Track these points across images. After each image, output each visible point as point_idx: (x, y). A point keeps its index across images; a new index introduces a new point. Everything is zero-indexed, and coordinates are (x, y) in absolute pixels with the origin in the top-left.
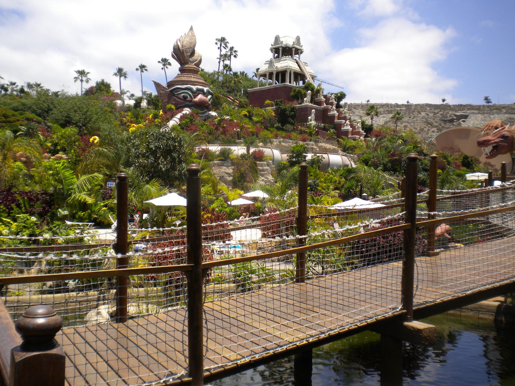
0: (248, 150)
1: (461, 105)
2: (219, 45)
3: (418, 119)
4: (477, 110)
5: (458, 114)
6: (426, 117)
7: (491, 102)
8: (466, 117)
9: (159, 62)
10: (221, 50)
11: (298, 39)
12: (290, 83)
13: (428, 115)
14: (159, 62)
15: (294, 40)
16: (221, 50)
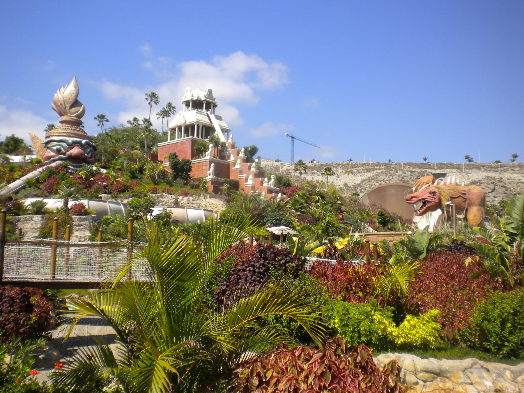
0: (66, 203)
1: (442, 164)
2: (149, 101)
3: (395, 177)
4: (456, 168)
5: (436, 172)
6: (403, 175)
7: (473, 161)
8: (444, 175)
9: (95, 118)
10: (151, 106)
11: (210, 92)
12: (202, 137)
13: (405, 173)
14: (95, 118)
15: (206, 93)
16: (151, 106)
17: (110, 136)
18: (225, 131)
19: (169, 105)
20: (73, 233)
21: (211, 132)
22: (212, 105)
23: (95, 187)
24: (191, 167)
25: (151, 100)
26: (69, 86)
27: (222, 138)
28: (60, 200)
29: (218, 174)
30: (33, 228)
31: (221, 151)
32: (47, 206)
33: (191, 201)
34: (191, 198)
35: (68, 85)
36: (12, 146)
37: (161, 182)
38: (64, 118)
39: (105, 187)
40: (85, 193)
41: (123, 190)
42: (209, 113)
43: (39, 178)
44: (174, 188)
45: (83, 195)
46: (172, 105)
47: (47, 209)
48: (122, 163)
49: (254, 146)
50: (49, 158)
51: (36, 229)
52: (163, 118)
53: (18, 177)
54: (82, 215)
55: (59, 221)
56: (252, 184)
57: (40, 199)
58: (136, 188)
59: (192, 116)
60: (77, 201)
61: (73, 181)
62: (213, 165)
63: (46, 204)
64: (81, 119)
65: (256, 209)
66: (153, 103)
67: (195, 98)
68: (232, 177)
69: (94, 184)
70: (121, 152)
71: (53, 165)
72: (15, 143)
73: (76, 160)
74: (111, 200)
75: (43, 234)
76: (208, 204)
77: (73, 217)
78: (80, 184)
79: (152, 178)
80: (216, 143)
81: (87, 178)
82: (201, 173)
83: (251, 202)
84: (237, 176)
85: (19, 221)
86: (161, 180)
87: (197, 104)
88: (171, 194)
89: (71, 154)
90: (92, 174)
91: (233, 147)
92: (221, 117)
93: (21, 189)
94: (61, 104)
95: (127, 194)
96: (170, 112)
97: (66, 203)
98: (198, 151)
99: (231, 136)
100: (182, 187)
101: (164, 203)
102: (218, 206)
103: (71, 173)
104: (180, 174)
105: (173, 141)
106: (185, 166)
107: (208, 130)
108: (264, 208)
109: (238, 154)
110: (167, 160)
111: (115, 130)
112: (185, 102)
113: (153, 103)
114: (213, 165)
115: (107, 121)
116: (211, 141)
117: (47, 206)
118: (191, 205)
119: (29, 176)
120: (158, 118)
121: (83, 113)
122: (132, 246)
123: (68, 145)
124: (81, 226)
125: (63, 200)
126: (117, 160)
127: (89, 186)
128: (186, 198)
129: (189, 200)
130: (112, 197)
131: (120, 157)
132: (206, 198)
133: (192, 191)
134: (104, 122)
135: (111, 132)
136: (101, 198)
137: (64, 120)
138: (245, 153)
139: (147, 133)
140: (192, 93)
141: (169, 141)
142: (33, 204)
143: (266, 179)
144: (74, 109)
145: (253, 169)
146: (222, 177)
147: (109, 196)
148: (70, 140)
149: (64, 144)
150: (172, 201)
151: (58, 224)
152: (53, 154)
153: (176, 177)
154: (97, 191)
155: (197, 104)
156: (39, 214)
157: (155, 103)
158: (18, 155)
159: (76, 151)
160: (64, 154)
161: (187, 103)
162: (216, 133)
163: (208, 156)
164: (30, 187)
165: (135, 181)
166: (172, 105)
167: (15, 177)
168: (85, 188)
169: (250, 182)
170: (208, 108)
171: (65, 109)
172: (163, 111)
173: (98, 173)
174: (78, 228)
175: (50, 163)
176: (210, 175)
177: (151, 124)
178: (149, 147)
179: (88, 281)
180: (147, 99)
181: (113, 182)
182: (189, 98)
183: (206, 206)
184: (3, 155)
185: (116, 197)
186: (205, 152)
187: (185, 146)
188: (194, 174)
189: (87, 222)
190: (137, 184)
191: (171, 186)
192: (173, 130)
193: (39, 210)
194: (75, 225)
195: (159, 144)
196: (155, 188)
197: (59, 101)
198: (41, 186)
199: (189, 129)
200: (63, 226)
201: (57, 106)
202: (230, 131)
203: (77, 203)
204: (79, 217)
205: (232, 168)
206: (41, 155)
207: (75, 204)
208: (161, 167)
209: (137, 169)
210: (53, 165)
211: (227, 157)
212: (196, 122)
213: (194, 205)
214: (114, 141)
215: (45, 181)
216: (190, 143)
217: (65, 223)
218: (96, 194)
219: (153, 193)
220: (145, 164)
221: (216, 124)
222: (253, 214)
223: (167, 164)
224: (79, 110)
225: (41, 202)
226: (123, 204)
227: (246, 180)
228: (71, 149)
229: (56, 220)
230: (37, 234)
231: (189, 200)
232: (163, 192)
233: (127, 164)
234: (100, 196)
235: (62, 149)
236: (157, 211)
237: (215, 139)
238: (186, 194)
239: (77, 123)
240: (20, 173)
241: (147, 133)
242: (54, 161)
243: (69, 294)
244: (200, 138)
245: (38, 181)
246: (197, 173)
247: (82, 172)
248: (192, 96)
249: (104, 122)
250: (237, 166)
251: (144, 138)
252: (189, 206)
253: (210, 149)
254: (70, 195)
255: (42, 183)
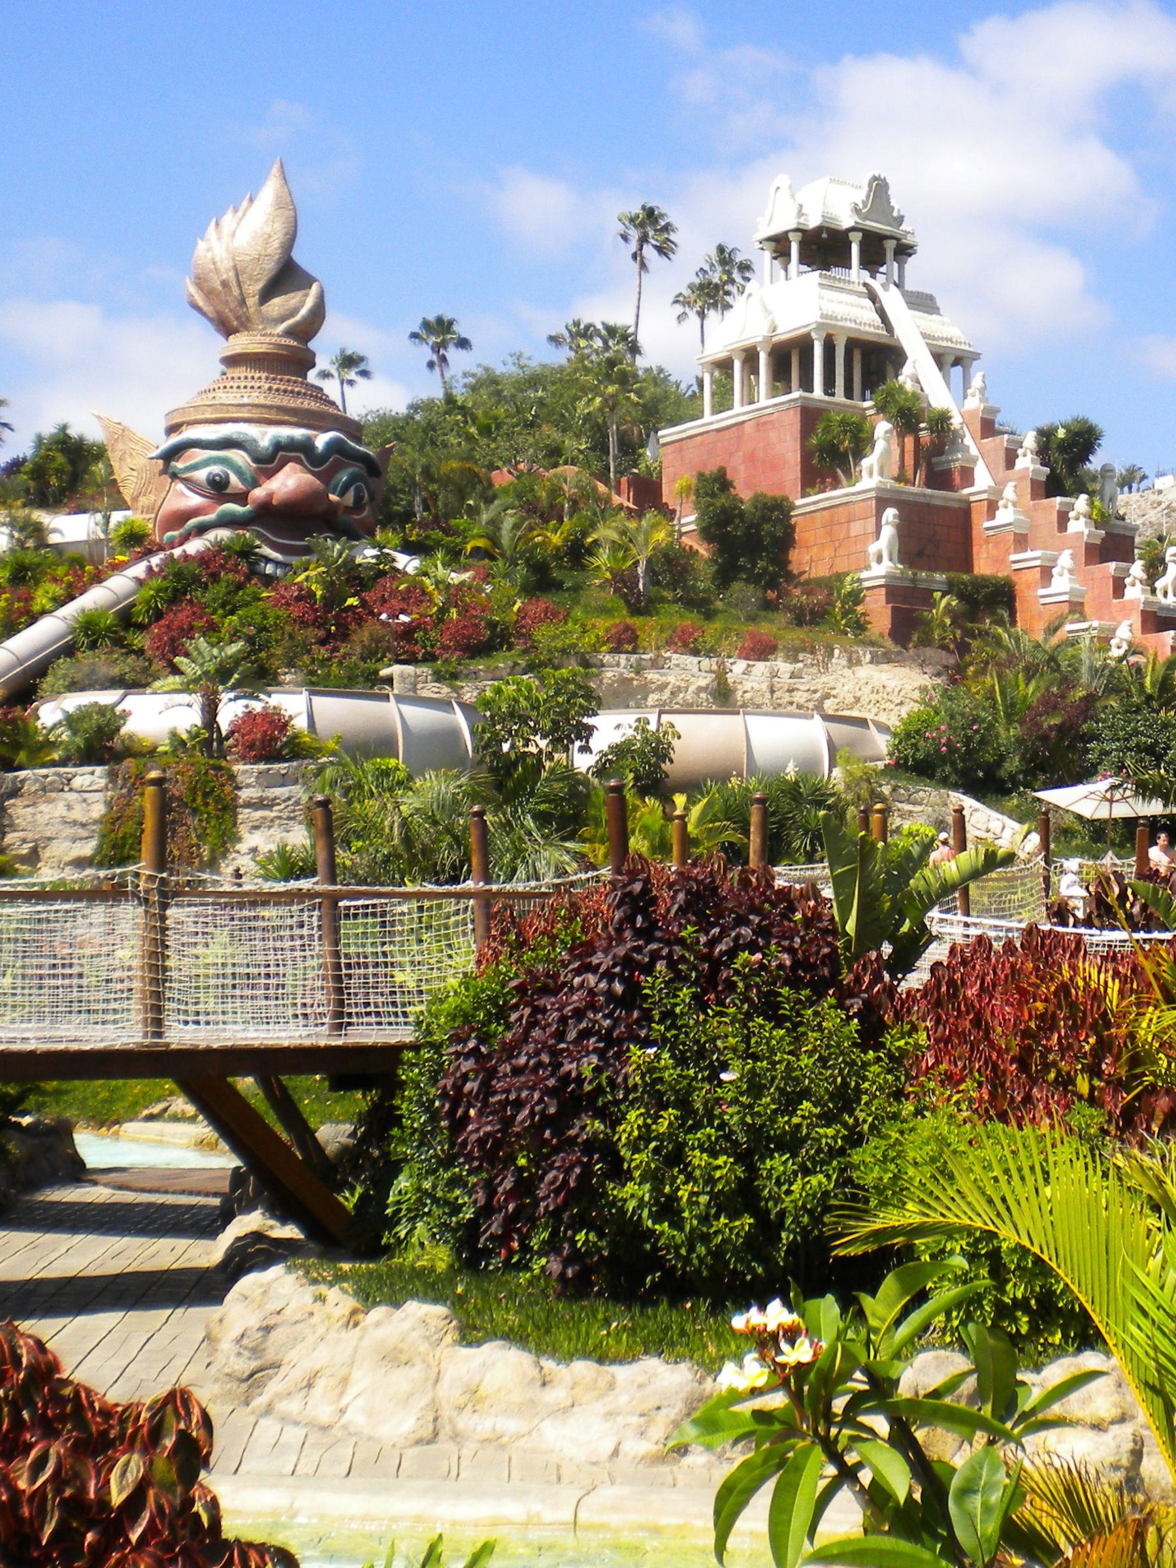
0: (211, 710)
2: (633, 246)
9: (414, 336)
10: (643, 266)
11: (879, 188)
12: (849, 394)
14: (414, 336)
15: (860, 195)
17: (463, 409)
18: (950, 360)
19: (725, 257)
20: (239, 840)
21: (890, 370)
22: (890, 245)
23: (363, 635)
24: (792, 528)
25: (644, 239)
26: (256, 203)
27: (937, 392)
28: (185, 698)
29: (920, 554)
30: (75, 823)
31: (932, 447)
32: (130, 727)
33: (785, 680)
34: (783, 667)
35: (251, 200)
36: (58, 471)
37: (663, 600)
38: (242, 343)
39: (407, 633)
40: (325, 662)
41: (483, 642)
42: (876, 284)
43: (133, 605)
44: (718, 625)
45: (312, 673)
46: (739, 258)
47: (131, 737)
48: (495, 523)
49: (1085, 421)
50: (180, 518)
51: (83, 825)
52: (702, 315)
53: (48, 606)
54: (277, 758)
55: (177, 789)
56: (1071, 592)
57: (107, 698)
58: (543, 634)
59: (792, 302)
60: (257, 698)
61: (271, 614)
62: (890, 513)
63: (125, 715)
64: (312, 345)
65: (1050, 704)
66: (649, 252)
67: (813, 222)
68: (983, 566)
69: (360, 621)
70: (502, 478)
71: (194, 547)
72: (72, 462)
73: (292, 520)
74: (431, 689)
75: (114, 847)
76: (867, 690)
77: (238, 768)
78: (304, 624)
79: (623, 581)
80: (907, 415)
81: (334, 597)
82: (842, 551)
83: (1031, 672)
84: (1002, 561)
85: (15, 793)
86: (665, 595)
87: (823, 248)
88: (695, 652)
89: (270, 495)
90: (358, 578)
91: (988, 428)
92: (931, 298)
93: (56, 655)
94: (225, 284)
95: (502, 661)
96: (734, 289)
97: (211, 710)
98: (830, 454)
99: (977, 382)
100: (752, 618)
101: (666, 694)
102: (890, 692)
103: (268, 580)
104: (742, 561)
105: (726, 418)
106: (767, 527)
107: (875, 360)
108: (1090, 699)
109: (1010, 459)
110: (689, 505)
111: (489, 383)
112: (769, 239)
113: (649, 252)
114: (890, 513)
115: (463, 343)
116: (881, 409)
117: (130, 727)
118: (787, 698)
119: (94, 598)
120: (681, 318)
121: (318, 314)
122: (163, 895)
123: (256, 460)
124: (269, 807)
125: (197, 699)
126: (473, 512)
127: (342, 637)
128: (761, 667)
129: (774, 675)
130: (439, 677)
131: (489, 501)
132: (859, 663)
133: (797, 635)
134: (452, 353)
135: (474, 388)
136: (389, 680)
137: (239, 350)
138: (1043, 452)
139: (611, 389)
140: (800, 197)
141: (708, 417)
142: (71, 721)
143: (1137, 569)
144: (277, 304)
145: (1078, 526)
146: (932, 568)
147: (425, 670)
148: (265, 436)
149: (239, 457)
150: (703, 683)
151: (164, 806)
152: (195, 500)
153: (725, 575)
154: (374, 653)
155: (823, 248)
156: (100, 762)
157: (661, 250)
158: (85, 512)
159: (289, 481)
160: (241, 498)
161: (779, 245)
162: (907, 370)
163: (874, 472)
164: (93, 646)
165: (548, 600)
166: (739, 258)
167: (36, 608)
168: (322, 642)
169: (1062, 584)
170: (873, 259)
171: (243, 302)
172: (702, 287)
173: (383, 572)
174: (259, 814)
175: (185, 539)
176: (879, 559)
177: (635, 349)
178: (630, 448)
179: (61, 1047)
180: (625, 238)
181: (443, 610)
182: (784, 222)
183: (858, 700)
184: (22, 513)
185: (455, 676)
186: (859, 454)
187: (773, 435)
188: (810, 559)
189: (298, 791)
190: (550, 615)
191: (709, 615)
192: (724, 366)
193: (100, 744)
194: (248, 805)
195: (667, 434)
196: (627, 628)
197: (217, 270)
198: (139, 640)
199: (788, 359)
200: (195, 811)
201: (209, 294)
202: (976, 356)
203: (257, 706)
204: (262, 767)
205: (982, 525)
206: (149, 509)
207: (249, 715)
208: (660, 536)
209: (558, 549)
210: (194, 547)
211: (957, 477)
212: (820, 326)
213: (800, 697)
214: (473, 430)
215: (158, 615)
216: (792, 423)
217: (206, 795)
218: (370, 665)
219: (617, 650)
220: (593, 525)
221: (910, 331)
222: (1039, 726)
223: (689, 520)
224: (303, 303)
225: (102, 710)
226: (462, 705)
227: (1046, 573)
228: (270, 474)
229: (158, 782)
230: (87, 849)
231: (774, 675)
232: (669, 643)
233: (516, 527)
234: (384, 672)
235: (233, 478)
236: (610, 729)
237: (901, 399)
238: (761, 651)
239: (292, 361)
240: (57, 590)
241: (611, 389)
242: (202, 530)
243: (159, 1100)
244: (840, 397)
245: (126, 618)
246: (828, 553)
247: (312, 573)
248: (800, 213)
249: (452, 353)
250: (1005, 515)
251: (607, 404)
252: (777, 705)
253: (880, 446)
254: (223, 674)
255: (141, 627)
